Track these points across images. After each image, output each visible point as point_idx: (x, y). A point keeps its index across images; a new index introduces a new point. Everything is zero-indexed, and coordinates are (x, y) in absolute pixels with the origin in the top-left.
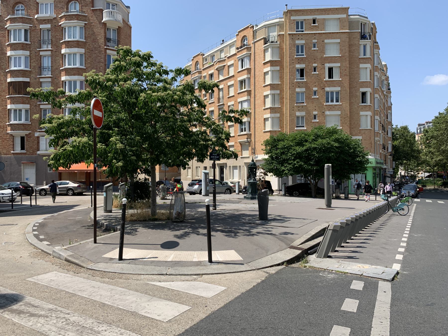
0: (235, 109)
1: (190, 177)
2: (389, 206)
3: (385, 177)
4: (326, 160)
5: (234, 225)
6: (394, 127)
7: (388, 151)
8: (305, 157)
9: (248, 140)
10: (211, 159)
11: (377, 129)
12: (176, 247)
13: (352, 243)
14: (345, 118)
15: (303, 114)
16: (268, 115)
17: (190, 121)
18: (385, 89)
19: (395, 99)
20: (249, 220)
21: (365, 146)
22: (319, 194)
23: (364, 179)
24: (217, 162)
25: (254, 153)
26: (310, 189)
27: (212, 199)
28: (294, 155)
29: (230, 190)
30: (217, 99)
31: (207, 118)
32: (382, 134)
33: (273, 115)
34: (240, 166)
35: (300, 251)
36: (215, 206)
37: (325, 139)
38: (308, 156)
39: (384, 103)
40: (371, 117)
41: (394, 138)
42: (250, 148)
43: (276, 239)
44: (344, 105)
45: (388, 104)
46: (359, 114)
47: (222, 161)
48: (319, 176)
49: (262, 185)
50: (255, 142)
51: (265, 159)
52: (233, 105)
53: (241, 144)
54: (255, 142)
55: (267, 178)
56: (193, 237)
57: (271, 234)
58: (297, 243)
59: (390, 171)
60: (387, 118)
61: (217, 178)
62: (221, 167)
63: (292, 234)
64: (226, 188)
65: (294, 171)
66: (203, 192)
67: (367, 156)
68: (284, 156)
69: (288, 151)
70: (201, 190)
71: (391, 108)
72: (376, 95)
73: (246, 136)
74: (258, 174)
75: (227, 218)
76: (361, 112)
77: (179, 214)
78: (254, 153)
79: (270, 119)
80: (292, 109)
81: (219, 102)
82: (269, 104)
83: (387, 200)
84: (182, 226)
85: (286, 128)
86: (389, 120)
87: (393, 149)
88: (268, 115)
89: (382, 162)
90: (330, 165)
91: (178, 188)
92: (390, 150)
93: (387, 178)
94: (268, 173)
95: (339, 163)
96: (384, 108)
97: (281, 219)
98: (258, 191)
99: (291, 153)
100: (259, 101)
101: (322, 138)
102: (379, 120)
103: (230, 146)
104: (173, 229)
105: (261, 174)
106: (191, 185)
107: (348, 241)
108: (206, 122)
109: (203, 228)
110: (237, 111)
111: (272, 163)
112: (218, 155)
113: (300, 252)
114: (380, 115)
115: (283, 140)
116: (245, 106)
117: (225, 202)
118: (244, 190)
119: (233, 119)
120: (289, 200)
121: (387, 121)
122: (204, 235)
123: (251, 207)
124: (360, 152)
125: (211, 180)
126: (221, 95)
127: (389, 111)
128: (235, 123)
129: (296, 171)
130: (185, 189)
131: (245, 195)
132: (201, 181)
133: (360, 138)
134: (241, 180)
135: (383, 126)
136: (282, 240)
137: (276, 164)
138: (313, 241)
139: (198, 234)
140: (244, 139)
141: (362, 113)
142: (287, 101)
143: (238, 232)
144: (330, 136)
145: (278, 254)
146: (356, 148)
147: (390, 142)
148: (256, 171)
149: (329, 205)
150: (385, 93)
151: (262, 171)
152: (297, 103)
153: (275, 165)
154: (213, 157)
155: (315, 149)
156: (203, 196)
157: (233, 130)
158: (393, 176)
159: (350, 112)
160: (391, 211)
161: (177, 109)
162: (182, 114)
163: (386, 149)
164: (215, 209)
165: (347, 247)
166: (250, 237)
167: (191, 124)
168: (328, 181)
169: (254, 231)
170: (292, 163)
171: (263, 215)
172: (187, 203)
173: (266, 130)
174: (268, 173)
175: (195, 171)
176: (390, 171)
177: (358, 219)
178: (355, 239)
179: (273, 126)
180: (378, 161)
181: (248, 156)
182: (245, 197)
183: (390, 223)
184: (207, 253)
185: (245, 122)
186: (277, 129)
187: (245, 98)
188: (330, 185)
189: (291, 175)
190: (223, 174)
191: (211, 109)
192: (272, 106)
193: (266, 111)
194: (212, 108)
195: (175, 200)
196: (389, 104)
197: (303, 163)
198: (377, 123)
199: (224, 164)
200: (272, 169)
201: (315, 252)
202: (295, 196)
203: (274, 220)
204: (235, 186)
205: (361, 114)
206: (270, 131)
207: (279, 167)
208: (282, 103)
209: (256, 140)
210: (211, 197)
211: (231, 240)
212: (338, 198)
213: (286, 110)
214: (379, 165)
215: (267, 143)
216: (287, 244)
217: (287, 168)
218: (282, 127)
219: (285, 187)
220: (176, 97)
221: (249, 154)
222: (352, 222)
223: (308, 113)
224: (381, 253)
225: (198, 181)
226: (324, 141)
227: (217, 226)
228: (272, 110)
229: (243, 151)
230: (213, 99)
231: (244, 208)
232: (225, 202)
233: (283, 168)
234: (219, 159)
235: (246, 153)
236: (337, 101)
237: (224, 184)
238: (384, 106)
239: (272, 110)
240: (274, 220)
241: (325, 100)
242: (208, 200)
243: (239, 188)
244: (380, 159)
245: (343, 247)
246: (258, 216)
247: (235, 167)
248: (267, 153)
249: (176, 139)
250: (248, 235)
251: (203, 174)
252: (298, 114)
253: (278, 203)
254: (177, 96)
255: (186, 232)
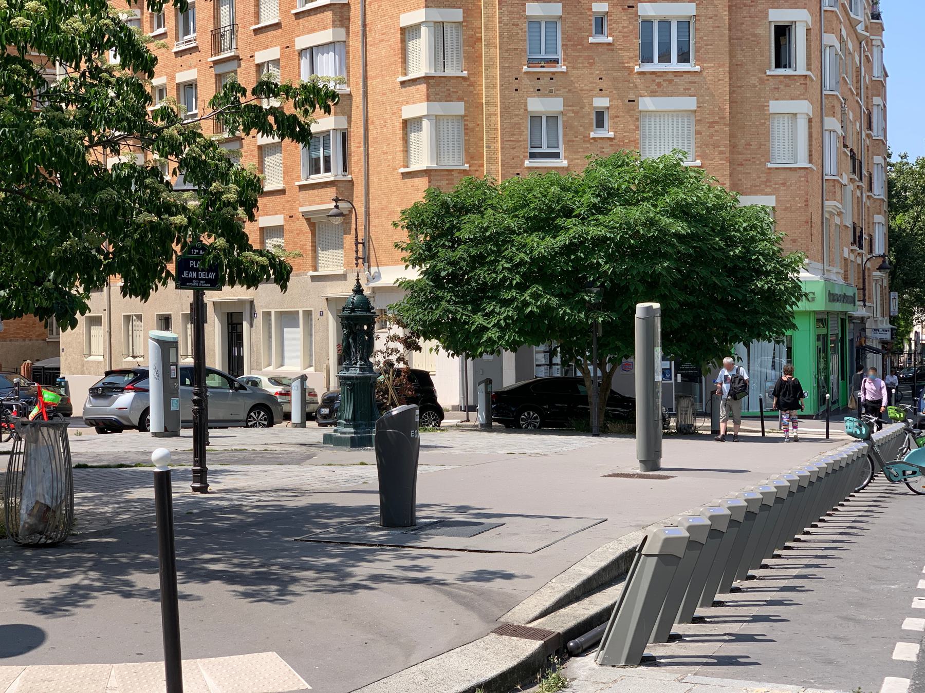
0: (278, 77)
1: (98, 357)
2: (873, 461)
3: (861, 351)
4: (641, 288)
5: (277, 549)
6: (895, 159)
7: (871, 251)
8: (564, 274)
9: (342, 205)
10: (182, 283)
11: (830, 167)
12: (30, 648)
13: (736, 604)
14: (711, 125)
15: (555, 105)
16: (417, 108)
17: (86, 124)
18: (860, 15)
19: (897, 53)
20: (342, 528)
21: (785, 234)
22: (616, 417)
23: (784, 361)
24: (210, 297)
25: (366, 260)
26: (585, 400)
27: (192, 447)
28: (523, 269)
29: (267, 411)
30: (208, 37)
31: (165, 114)
32: (851, 187)
33: (439, 108)
34: (308, 314)
35: (539, 643)
36: (201, 476)
37: (637, 204)
38: (576, 270)
39: (858, 71)
40: (810, 121)
41: (895, 201)
42: (349, 240)
43: (443, 598)
44: (709, 75)
45: (871, 75)
46: (764, 108)
47: (232, 293)
48: (617, 349)
49: (399, 389)
50: (368, 214)
51: (410, 285)
52: (276, 62)
53: (311, 220)
54: (368, 214)
55: (419, 361)
56: (107, 605)
57: (426, 581)
58: (523, 612)
59: (879, 328)
60: (870, 127)
61: (215, 359)
62: (230, 316)
63: (509, 577)
64: (250, 403)
65: (521, 332)
66: (155, 421)
67: (794, 270)
68: (482, 274)
69: (499, 252)
70: (146, 411)
71: (884, 87)
72: (830, 39)
73: (331, 192)
74: (379, 345)
75: (251, 524)
76: (772, 103)
77: (44, 512)
78: (364, 259)
79: (425, 123)
80: (513, 86)
81: (217, 49)
82: (421, 63)
83: (868, 438)
84: (60, 563)
85: (489, 158)
86: (876, 133)
87: (890, 245)
88: (417, 108)
89: (850, 294)
90: (656, 305)
91: (46, 405)
92: (880, 248)
93: (869, 355)
94: (421, 342)
95: (692, 299)
96: (858, 89)
97: (470, 522)
98: (380, 412)
99: (511, 259)
100: (382, 50)
101: (627, 203)
102: (840, 131)
103: (265, 232)
104: (25, 577)
105: (392, 345)
106: (102, 392)
107: (718, 597)
108: (159, 131)
109: (146, 567)
110: (288, 90)
111: (438, 299)
112: (216, 267)
113: (537, 644)
114: (843, 113)
115: (478, 209)
116: (327, 69)
117: (246, 458)
118: (325, 411)
119: (271, 119)
120: (503, 446)
121: (869, 136)
122: (151, 594)
123: (352, 475)
124: (769, 258)
125: (185, 372)
126: (225, 21)
127: (877, 100)
128: (282, 137)
129: (531, 329)
130: (77, 411)
131: (330, 430)
132: (142, 375)
133: (769, 201)
134: (312, 369)
135: (853, 157)
136: (468, 605)
137: (453, 302)
138: (586, 601)
139: (127, 595)
140: (324, 203)
141: (776, 106)
142: (491, 54)
143: (295, 580)
144: (657, 194)
145: (453, 659)
146: (753, 240)
147: (879, 218)
148: (370, 332)
149: (651, 461)
150: (860, 28)
151: (400, 332)
152: (530, 62)
153: (448, 306)
154: (193, 275)
155: (600, 242)
156: (156, 435)
157: (277, 167)
158: (891, 348)
159: (732, 102)
160: (881, 479)
161: (31, 72)
162: (55, 95)
163: (865, 244)
164: (204, 490)
165: (716, 620)
166: (339, 596)
167: (91, 139)
168: (647, 368)
169: (362, 570)
170: (513, 299)
171: (398, 508)
172: (85, 466)
173: (413, 168)
174: (421, 342)
175: (116, 333)
176: (879, 328)
177: (756, 510)
178: (748, 590)
179: (438, 150)
180: (837, 291)
181: (340, 271)
182: (328, 439)
183: (875, 525)
184: (160, 668)
185: (326, 135)
186: (455, 162)
187: (326, 36)
188: (655, 384)
189: (514, 346)
190: (240, 345)
191: (184, 76)
192: (432, 72)
193: (412, 89)
194: (181, 72)
195: (26, 454)
196: (877, 72)
197: (555, 301)
198: (831, 147)
199: (241, 302)
200: (438, 322)
201: (596, 644)
202: (527, 431)
203: (442, 524)
204: (287, 394)
205: (772, 110)
206: (427, 172)
207: (462, 313)
208: (473, 60)
209: (372, 207)
210: (185, 442)
211: (266, 611)
212: (686, 432)
213: (490, 90)
214: (838, 307)
215: (415, 220)
216: (485, 617)
217: (494, 321)
218: (473, 156)
219: (487, 393)
220: (19, 20)
221: (346, 264)
222: (733, 523)
223: (575, 102)
224: (840, 639)
225: (131, 377)
226: (635, 214)
227: (207, 556)
228: (436, 87)
229: (321, 254)
230: (192, 36)
231: (322, 480)
232: (246, 458)
233: (479, 320)
234: (215, 284)
235: (333, 261)
236: (684, 57)
237: (242, 387)
238: (858, 81)
239: (436, 87)
240: (442, 524)
241: (639, 52)
242: (159, 450)
243: (304, 403)
244: (842, 282)
245: (700, 620)
246: (377, 514)
247: (288, 318)
248: (417, 261)
249: (29, 198)
250: (334, 590)
251: (152, 344)
252: (536, 105)
253: (460, 460)
254: (28, 17)
255: (76, 587)
